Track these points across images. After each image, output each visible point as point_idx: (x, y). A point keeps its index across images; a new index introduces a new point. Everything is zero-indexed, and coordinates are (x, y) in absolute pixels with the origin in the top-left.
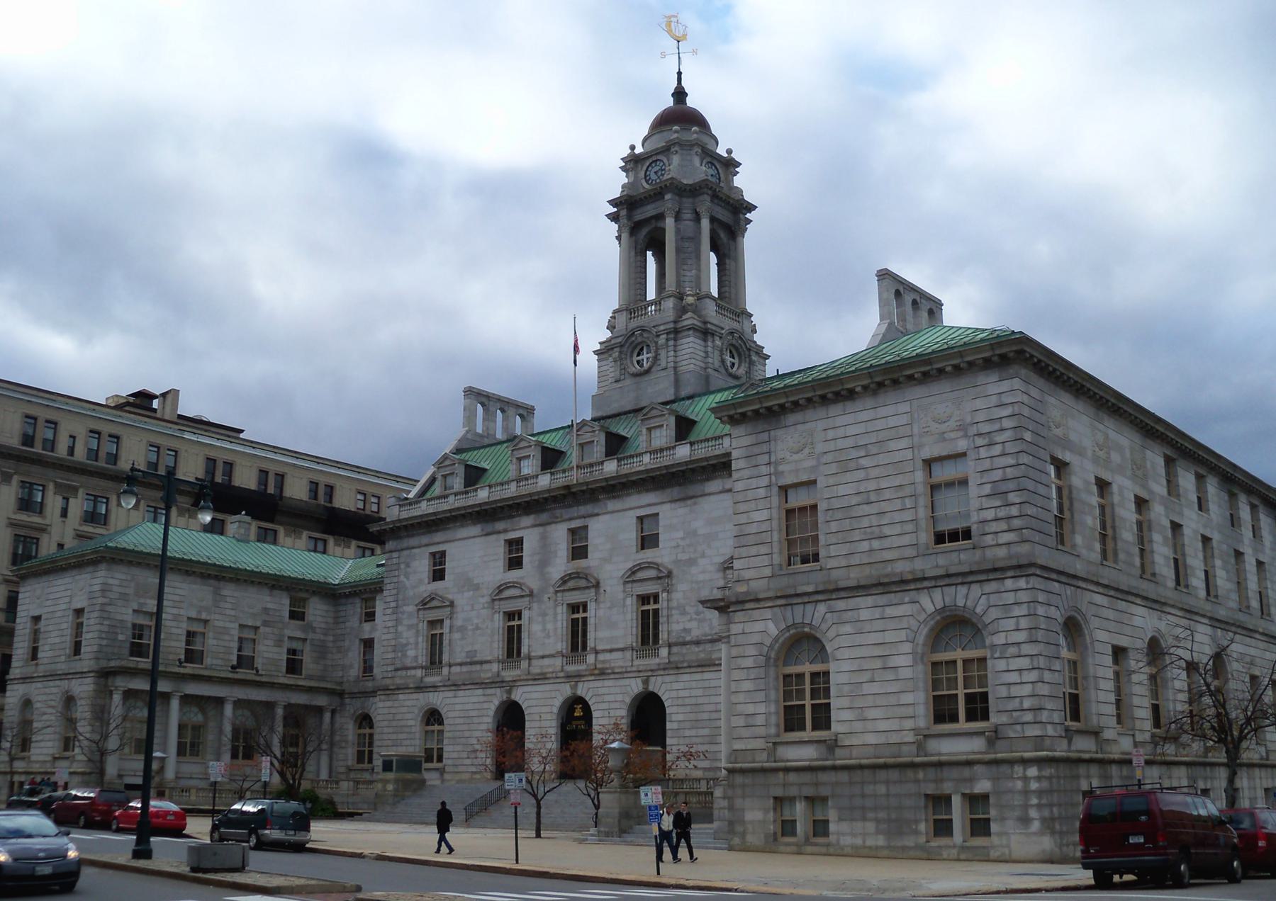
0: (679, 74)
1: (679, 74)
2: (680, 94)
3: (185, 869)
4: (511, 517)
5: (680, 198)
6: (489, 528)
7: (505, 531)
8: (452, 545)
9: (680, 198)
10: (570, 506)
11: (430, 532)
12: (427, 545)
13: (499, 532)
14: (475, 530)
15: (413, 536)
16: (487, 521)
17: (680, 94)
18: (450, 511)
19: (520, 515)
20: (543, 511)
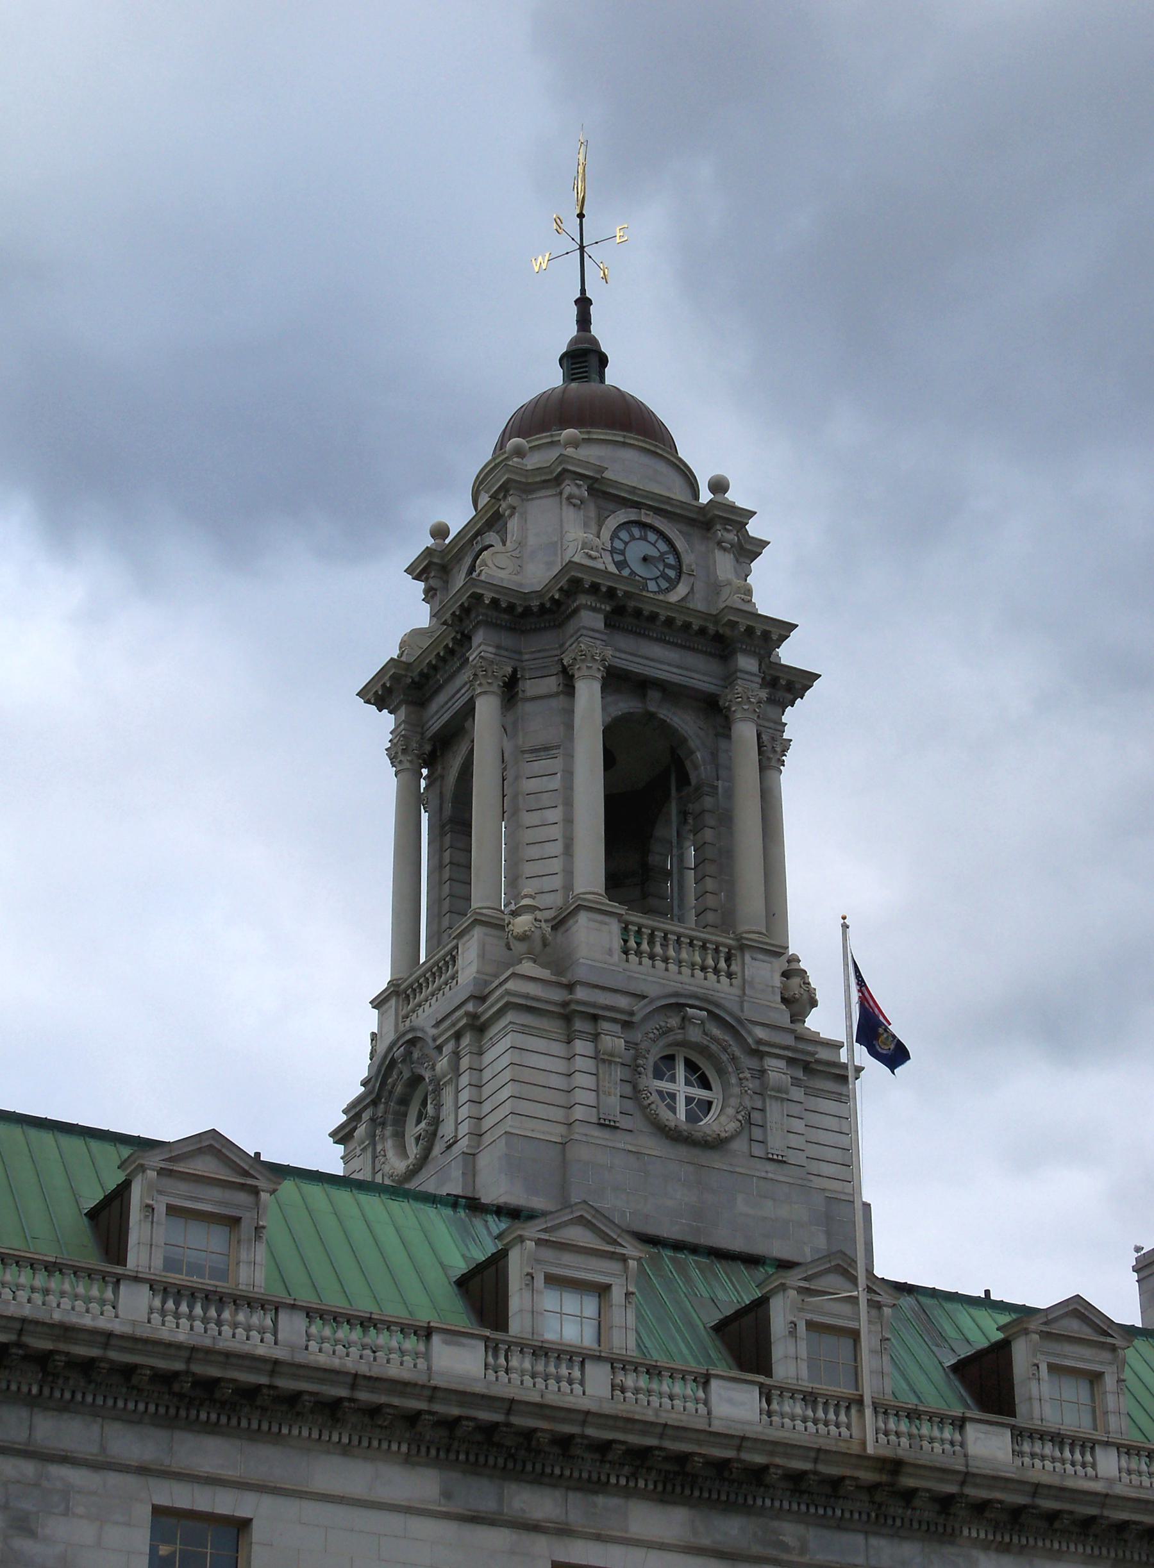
0: (584, 303)
1: (584, 303)
2: (584, 359)
3: (595, 1120)
4: (596, 1486)
5: (987, 1292)
6: (481, 1494)
7: (563, 1531)
8: (291, 1508)
9: (987, 1292)
10: (841, 1525)
11: (169, 1423)
12: (143, 1470)
13: (535, 1528)
14: (421, 1484)
15: (65, 1408)
16: (474, 1468)
17: (584, 359)
18: (274, 1366)
19: (628, 1493)
20: (729, 1507)
